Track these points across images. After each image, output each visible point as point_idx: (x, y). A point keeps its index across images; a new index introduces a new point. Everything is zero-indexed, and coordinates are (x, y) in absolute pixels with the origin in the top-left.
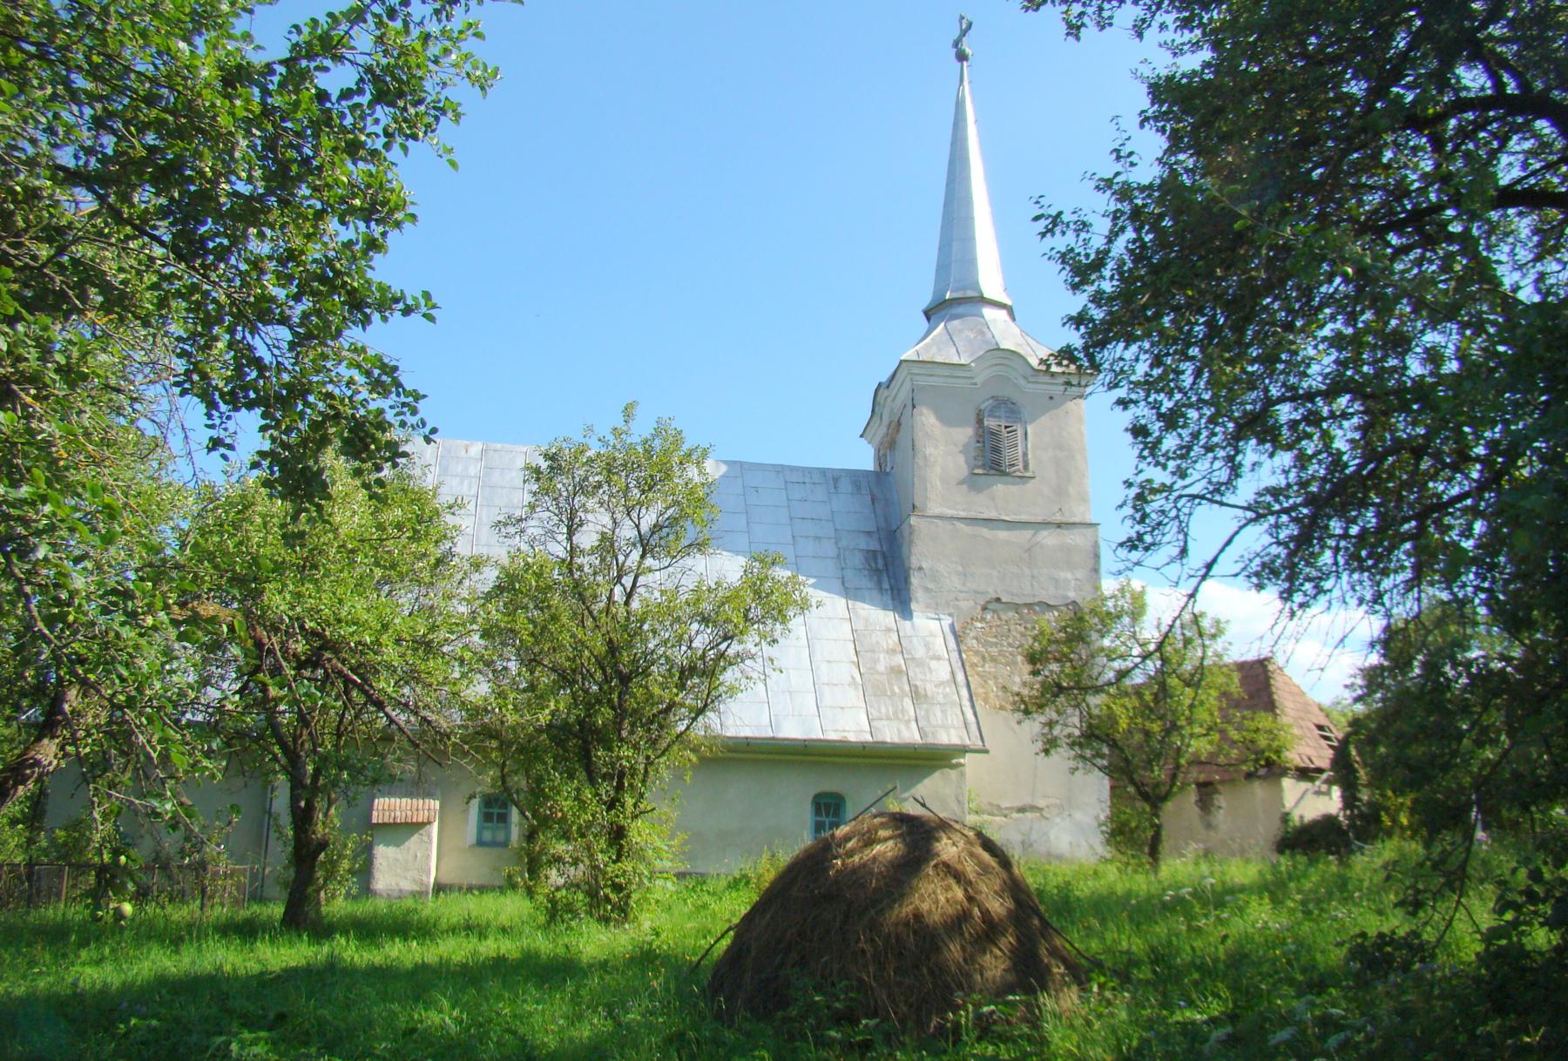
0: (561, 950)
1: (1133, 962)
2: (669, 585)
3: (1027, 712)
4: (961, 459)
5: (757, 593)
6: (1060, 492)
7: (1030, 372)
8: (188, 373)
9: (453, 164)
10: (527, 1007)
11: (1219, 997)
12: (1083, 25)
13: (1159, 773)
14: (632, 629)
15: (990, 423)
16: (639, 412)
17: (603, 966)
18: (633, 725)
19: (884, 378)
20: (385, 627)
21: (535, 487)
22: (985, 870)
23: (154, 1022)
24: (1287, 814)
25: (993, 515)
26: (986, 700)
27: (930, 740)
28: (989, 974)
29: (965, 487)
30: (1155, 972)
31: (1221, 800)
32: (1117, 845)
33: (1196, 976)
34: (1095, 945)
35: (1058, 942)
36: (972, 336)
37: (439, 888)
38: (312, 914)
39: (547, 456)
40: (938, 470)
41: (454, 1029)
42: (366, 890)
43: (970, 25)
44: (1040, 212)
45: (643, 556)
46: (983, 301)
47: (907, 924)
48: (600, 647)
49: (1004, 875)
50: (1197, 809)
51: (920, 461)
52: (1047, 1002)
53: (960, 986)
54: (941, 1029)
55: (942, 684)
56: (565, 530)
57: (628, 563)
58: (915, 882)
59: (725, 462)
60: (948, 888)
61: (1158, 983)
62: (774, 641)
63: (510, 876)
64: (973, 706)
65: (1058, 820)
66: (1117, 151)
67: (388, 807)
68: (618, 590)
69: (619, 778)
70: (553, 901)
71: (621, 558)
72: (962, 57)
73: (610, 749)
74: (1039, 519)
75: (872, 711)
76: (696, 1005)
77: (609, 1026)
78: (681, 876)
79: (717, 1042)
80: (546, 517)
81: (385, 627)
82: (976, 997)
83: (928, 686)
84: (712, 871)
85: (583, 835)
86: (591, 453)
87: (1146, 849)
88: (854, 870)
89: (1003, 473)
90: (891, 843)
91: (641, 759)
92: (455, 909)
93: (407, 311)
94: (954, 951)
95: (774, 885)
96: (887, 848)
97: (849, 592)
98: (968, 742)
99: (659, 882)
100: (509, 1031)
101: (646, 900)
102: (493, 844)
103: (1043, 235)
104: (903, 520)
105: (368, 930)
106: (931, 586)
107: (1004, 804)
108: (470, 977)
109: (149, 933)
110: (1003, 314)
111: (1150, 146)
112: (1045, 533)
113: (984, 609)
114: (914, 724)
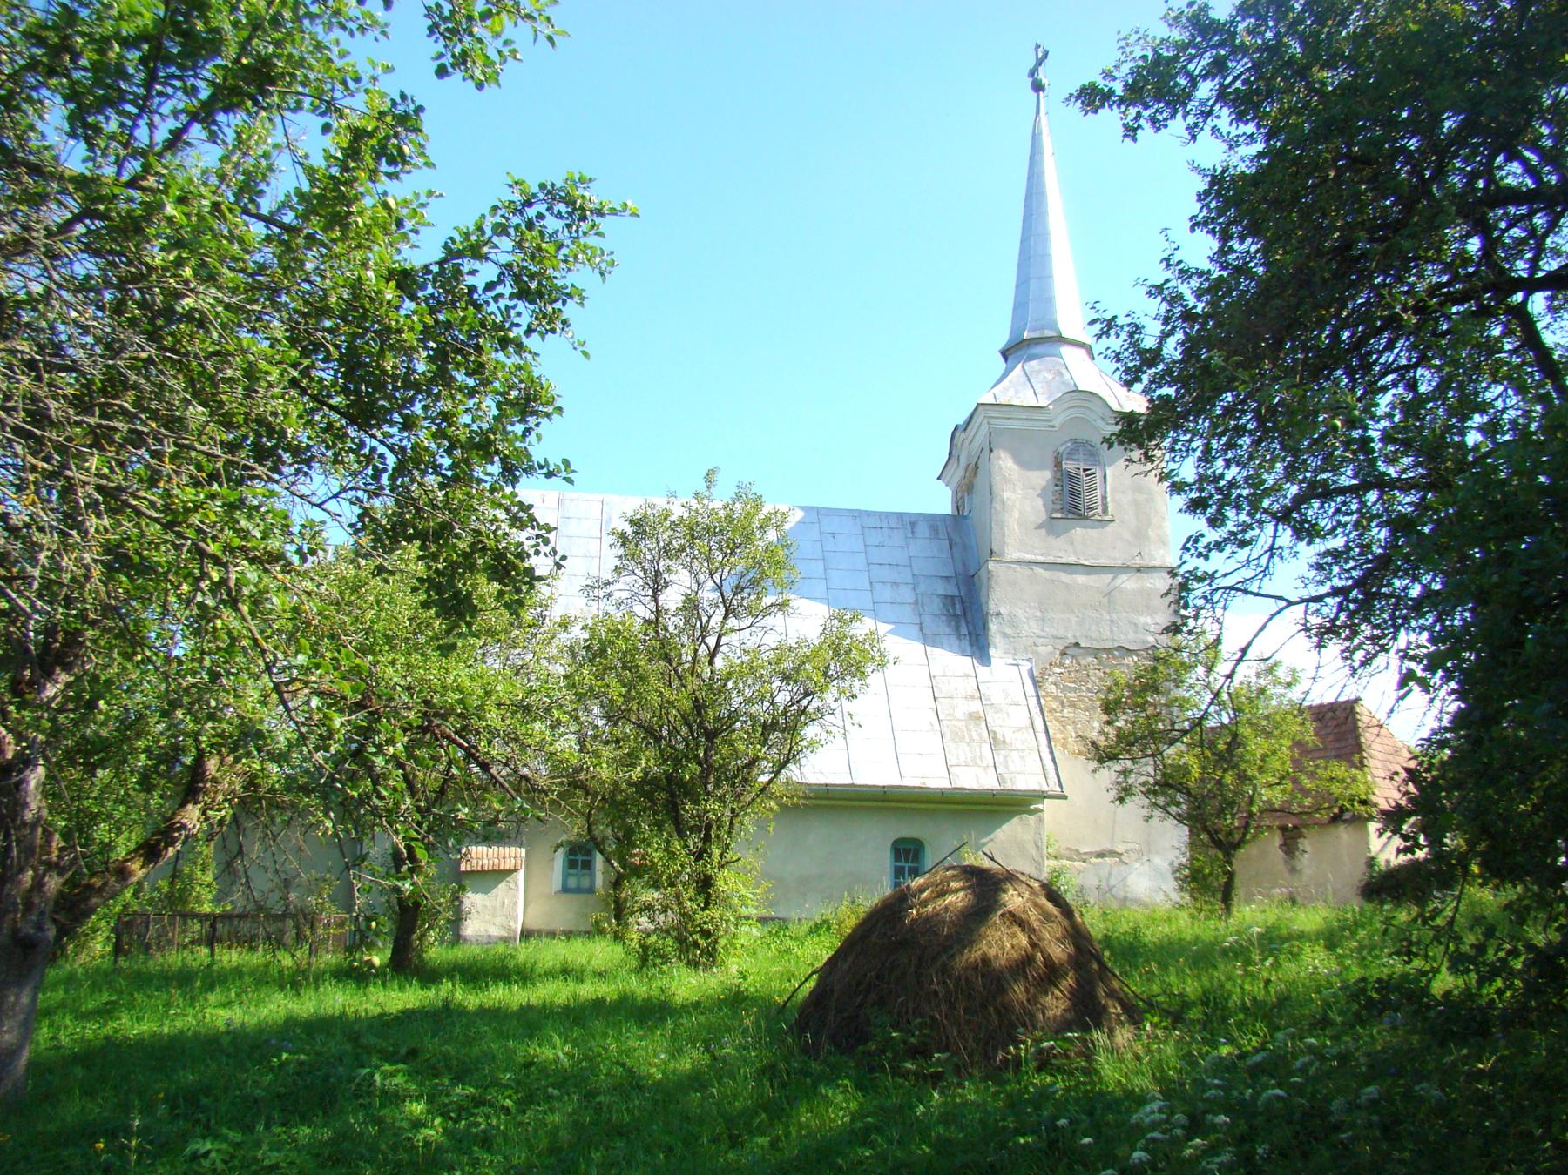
0: (655, 993)
1: (1186, 1005)
2: (750, 645)
3: (1101, 761)
4: (1040, 502)
6: (1140, 535)
8: (361, 517)
9: (585, 354)
10: (631, 1043)
13: (1231, 821)
15: (1069, 466)
16: (719, 477)
17: (696, 1005)
18: (718, 779)
19: (961, 421)
20: (488, 694)
21: (621, 552)
22: (1047, 917)
23: (303, 1057)
24: (1373, 859)
25: (1072, 559)
26: (1064, 745)
27: (1009, 786)
28: (1050, 1013)
29: (1043, 531)
30: (1205, 1014)
31: (1305, 844)
33: (1241, 1016)
34: (1156, 988)
35: (1116, 984)
37: (527, 934)
38: (416, 960)
39: (632, 522)
40: (1016, 514)
41: (566, 1062)
42: (458, 939)
43: (1046, 54)
44: (1095, 316)
45: (726, 617)
46: (1060, 340)
47: (976, 968)
48: (687, 705)
49: (1066, 922)
50: (1280, 852)
51: (998, 506)
52: (1099, 1037)
53: (1024, 1024)
54: (1005, 1061)
56: (650, 592)
58: (983, 930)
59: (801, 508)
60: (1014, 936)
61: (1205, 1024)
62: (854, 696)
63: (597, 922)
64: (1052, 753)
66: (1167, 260)
67: (482, 856)
68: (703, 650)
69: (706, 830)
70: (644, 947)
71: (704, 619)
72: (1038, 87)
73: (696, 802)
74: (1119, 563)
75: (952, 760)
76: (784, 1041)
78: (763, 920)
79: (805, 1072)
80: (632, 581)
81: (488, 694)
82: (1038, 1034)
84: (793, 915)
85: (672, 885)
86: (673, 518)
87: (1219, 896)
88: (928, 919)
90: (961, 894)
91: (727, 812)
92: (552, 953)
93: (549, 475)
94: (1018, 992)
95: (855, 930)
96: (957, 899)
97: (928, 638)
98: (1045, 788)
99: (745, 929)
100: (617, 1063)
101: (732, 944)
102: (578, 890)
104: (982, 564)
105: (474, 974)
106: (1009, 631)
108: (576, 1016)
109: (264, 979)
110: (1082, 352)
111: (1200, 250)
112: (1124, 577)
113: (1063, 654)
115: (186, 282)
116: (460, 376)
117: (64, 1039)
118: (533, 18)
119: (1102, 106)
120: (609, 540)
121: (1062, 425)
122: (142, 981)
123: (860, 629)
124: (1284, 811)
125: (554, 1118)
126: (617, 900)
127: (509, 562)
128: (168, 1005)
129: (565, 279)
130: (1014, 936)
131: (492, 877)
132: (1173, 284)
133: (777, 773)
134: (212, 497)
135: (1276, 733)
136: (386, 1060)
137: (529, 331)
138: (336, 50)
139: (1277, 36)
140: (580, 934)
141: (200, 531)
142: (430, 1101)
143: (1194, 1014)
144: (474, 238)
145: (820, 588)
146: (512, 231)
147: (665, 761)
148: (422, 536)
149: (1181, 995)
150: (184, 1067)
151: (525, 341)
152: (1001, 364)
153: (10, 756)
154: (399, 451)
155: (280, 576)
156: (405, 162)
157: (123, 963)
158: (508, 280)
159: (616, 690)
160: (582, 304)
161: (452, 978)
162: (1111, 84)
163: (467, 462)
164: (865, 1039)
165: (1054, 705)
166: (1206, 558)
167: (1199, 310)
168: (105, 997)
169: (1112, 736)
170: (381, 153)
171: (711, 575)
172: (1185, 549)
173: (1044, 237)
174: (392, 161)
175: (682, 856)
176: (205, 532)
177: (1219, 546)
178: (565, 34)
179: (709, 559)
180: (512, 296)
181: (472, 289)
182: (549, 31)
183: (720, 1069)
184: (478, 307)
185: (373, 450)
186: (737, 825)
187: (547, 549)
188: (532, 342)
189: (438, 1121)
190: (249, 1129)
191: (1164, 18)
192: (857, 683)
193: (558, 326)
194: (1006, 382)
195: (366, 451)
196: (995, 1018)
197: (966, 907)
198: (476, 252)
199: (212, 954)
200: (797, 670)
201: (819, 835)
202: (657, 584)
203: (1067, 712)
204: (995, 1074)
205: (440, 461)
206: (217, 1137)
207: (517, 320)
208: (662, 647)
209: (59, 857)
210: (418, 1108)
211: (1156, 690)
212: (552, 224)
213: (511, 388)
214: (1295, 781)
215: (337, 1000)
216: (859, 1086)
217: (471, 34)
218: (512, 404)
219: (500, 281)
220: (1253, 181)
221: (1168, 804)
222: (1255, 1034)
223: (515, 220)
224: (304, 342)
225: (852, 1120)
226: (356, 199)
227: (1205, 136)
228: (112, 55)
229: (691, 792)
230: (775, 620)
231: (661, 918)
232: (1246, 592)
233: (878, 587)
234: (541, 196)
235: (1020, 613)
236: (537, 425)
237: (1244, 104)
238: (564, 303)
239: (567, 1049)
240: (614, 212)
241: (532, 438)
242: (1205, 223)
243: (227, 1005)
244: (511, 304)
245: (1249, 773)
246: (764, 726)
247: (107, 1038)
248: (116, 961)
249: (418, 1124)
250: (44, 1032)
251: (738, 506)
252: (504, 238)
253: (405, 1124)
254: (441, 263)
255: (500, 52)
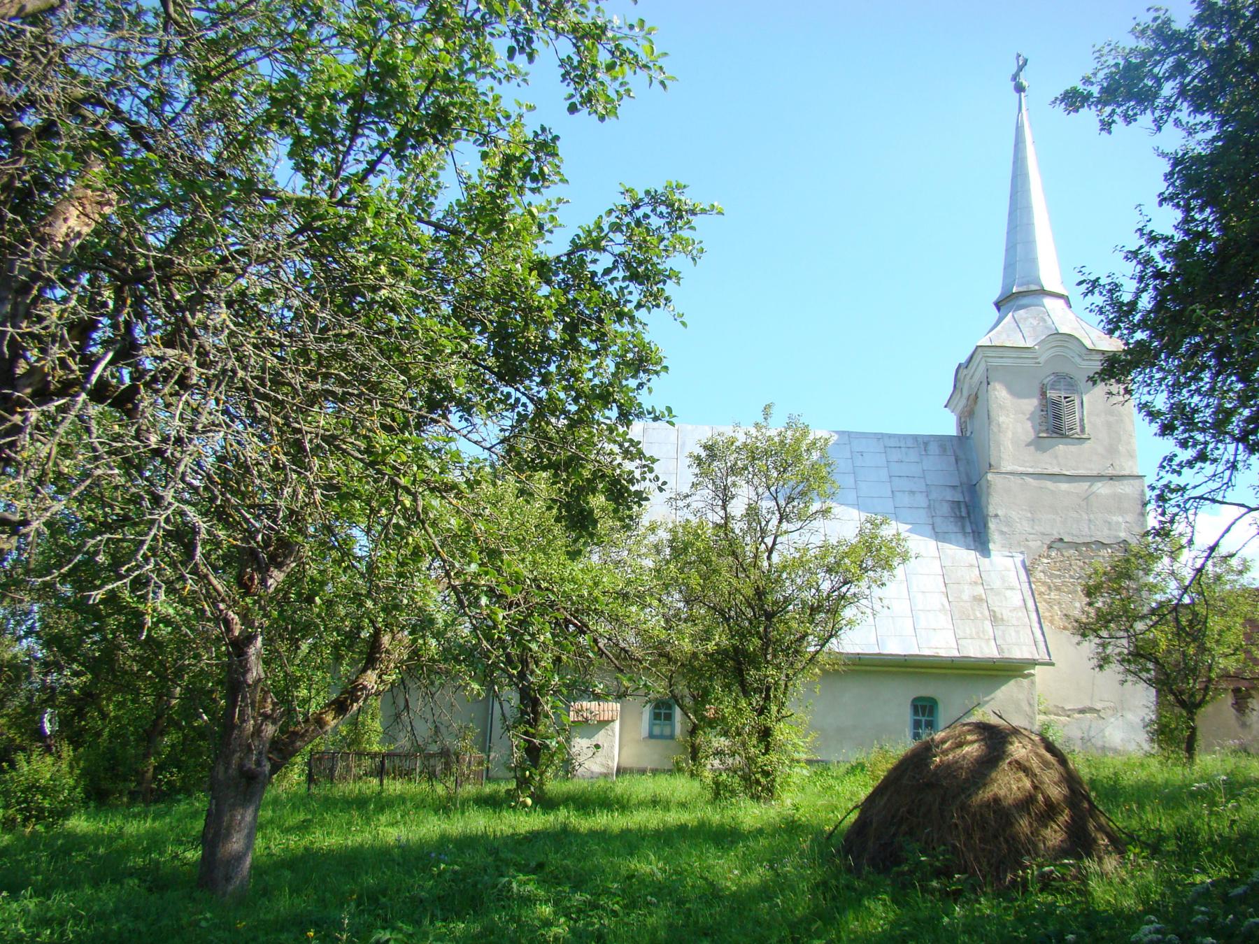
0: (727, 820)
1: (1162, 838)
3: (1084, 635)
4: (1029, 425)
5: (869, 549)
6: (1112, 450)
7: (1084, 351)
9: (684, 324)
10: (711, 862)
11: (1226, 866)
12: (1113, 121)
14: (774, 579)
15: (1052, 394)
16: (774, 411)
17: (760, 831)
18: (775, 650)
19: (963, 360)
20: (596, 584)
22: (1046, 764)
23: (456, 867)
25: (1056, 470)
26: (1052, 622)
27: (1006, 655)
29: (1032, 448)
30: (1179, 846)
32: (1159, 742)
33: (1210, 849)
34: (1134, 824)
35: (1103, 820)
36: (1035, 323)
37: (621, 771)
39: (705, 447)
40: (1009, 434)
41: (659, 876)
43: (1025, 62)
45: (780, 522)
46: (1044, 293)
48: (750, 592)
49: (1061, 769)
51: (994, 428)
52: (1091, 865)
53: (1028, 853)
54: (1013, 882)
55: (1015, 609)
56: (720, 503)
57: (770, 527)
58: (993, 775)
59: (837, 432)
60: (1019, 780)
63: (677, 763)
64: (1041, 628)
65: (1112, 720)
66: (1140, 230)
69: (766, 691)
70: (717, 783)
71: (763, 523)
72: (1020, 89)
74: (1095, 473)
77: (769, 874)
78: (809, 762)
79: (849, 887)
80: (707, 493)
81: (596, 584)
82: (1039, 860)
83: (1004, 612)
85: (739, 734)
86: (737, 444)
87: (1184, 746)
89: (1064, 436)
90: (976, 745)
92: (645, 787)
93: (656, 419)
94: (1024, 825)
96: (973, 749)
97: (939, 536)
98: (1037, 657)
99: (797, 770)
103: (1085, 295)
105: (583, 803)
106: (1005, 529)
107: (1067, 707)
108: (666, 838)
109: (421, 804)
110: (1061, 302)
111: (1167, 221)
112: (1099, 484)
113: (1050, 547)
114: (993, 642)
115: (382, 279)
116: (585, 342)
117: (275, 850)
118: (649, 68)
119: (1083, 106)
120: (688, 461)
121: (1046, 362)
122: (329, 803)
123: (887, 531)
124: (1237, 676)
125: (651, 921)
126: (693, 746)
127: (622, 486)
128: (349, 823)
129: (667, 264)
130: (1019, 780)
131: (590, 726)
132: (1146, 249)
133: (823, 646)
134: (404, 442)
135: (1231, 612)
136: (519, 871)
137: (639, 306)
138: (491, 95)
139: (1231, 41)
140: (664, 771)
141: (394, 468)
142: (556, 904)
143: (1170, 846)
144: (594, 234)
145: (852, 496)
146: (624, 229)
147: (733, 636)
148: (555, 466)
149: (1158, 830)
150: (367, 873)
151: (636, 314)
152: (995, 314)
153: (237, 634)
154: (537, 402)
155: (455, 502)
156: (544, 179)
157: (314, 790)
158: (621, 266)
159: (695, 581)
160: (678, 283)
161: (567, 806)
162: (1089, 88)
163: (589, 408)
164: (898, 863)
165: (1043, 589)
166: (1179, 473)
167: (1167, 270)
168: (302, 817)
169: (1092, 615)
170: (526, 172)
171: (768, 488)
172: (1162, 467)
173: (1028, 209)
174: (535, 179)
175: (748, 712)
176: (398, 470)
177: (1190, 464)
178: (673, 79)
179: (767, 477)
180: (624, 279)
181: (594, 274)
182: (662, 77)
183: (779, 884)
184: (597, 288)
185: (518, 400)
186: (790, 688)
187: (651, 476)
188: (641, 314)
189: (562, 920)
190: (418, 923)
191: (1132, 31)
192: (886, 573)
193: (662, 302)
194: (999, 328)
195: (512, 401)
196: (1004, 846)
197: (980, 756)
198: (597, 246)
199: (381, 784)
200: (838, 563)
201: (853, 693)
202: (725, 497)
203: (1054, 595)
204: (1003, 893)
205: (569, 408)
206: (393, 929)
207: (629, 298)
208: (731, 545)
209: (273, 710)
210: (546, 910)
211: (1130, 578)
212: (655, 222)
213: (627, 352)
214: (1248, 652)
215: (478, 822)
216: (894, 901)
217: (595, 79)
218: (628, 364)
219: (615, 267)
220: (1213, 160)
221: (1140, 671)
222: (1224, 865)
223: (627, 220)
224: (464, 314)
225: (892, 928)
226: (508, 209)
227: (1169, 127)
228: (325, 108)
229: (754, 661)
230: (818, 523)
231: (730, 761)
232: (1213, 501)
233: (897, 494)
234: (646, 200)
235: (1014, 514)
236: (649, 380)
237: (1200, 99)
238: (665, 283)
239: (660, 865)
240: (704, 211)
241: (645, 390)
242: (1171, 198)
243: (393, 824)
244: (624, 285)
245: (1208, 645)
246: (812, 608)
247: (306, 849)
248: (309, 789)
249: (547, 924)
250: (259, 843)
251: (789, 433)
252: (618, 234)
253: (536, 923)
254: (568, 255)
255: (617, 92)
